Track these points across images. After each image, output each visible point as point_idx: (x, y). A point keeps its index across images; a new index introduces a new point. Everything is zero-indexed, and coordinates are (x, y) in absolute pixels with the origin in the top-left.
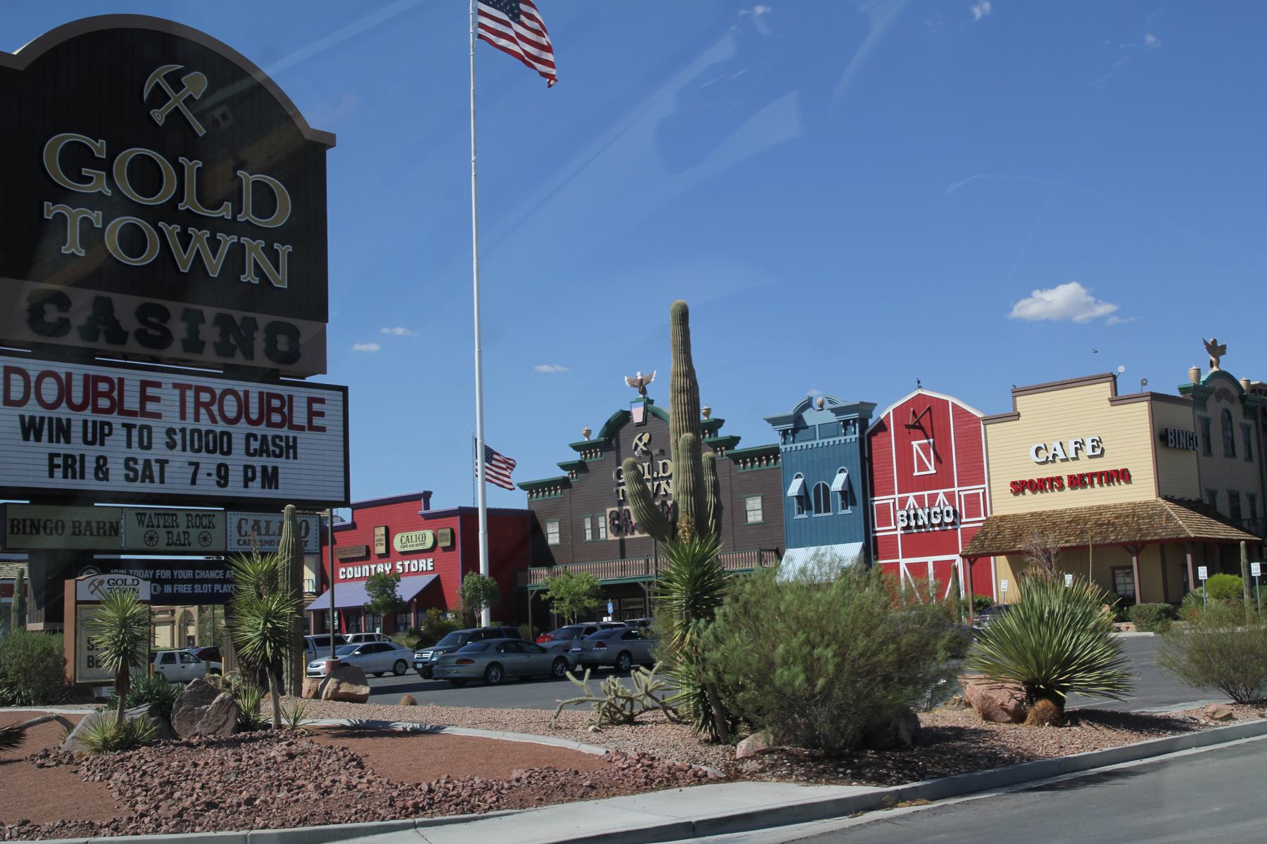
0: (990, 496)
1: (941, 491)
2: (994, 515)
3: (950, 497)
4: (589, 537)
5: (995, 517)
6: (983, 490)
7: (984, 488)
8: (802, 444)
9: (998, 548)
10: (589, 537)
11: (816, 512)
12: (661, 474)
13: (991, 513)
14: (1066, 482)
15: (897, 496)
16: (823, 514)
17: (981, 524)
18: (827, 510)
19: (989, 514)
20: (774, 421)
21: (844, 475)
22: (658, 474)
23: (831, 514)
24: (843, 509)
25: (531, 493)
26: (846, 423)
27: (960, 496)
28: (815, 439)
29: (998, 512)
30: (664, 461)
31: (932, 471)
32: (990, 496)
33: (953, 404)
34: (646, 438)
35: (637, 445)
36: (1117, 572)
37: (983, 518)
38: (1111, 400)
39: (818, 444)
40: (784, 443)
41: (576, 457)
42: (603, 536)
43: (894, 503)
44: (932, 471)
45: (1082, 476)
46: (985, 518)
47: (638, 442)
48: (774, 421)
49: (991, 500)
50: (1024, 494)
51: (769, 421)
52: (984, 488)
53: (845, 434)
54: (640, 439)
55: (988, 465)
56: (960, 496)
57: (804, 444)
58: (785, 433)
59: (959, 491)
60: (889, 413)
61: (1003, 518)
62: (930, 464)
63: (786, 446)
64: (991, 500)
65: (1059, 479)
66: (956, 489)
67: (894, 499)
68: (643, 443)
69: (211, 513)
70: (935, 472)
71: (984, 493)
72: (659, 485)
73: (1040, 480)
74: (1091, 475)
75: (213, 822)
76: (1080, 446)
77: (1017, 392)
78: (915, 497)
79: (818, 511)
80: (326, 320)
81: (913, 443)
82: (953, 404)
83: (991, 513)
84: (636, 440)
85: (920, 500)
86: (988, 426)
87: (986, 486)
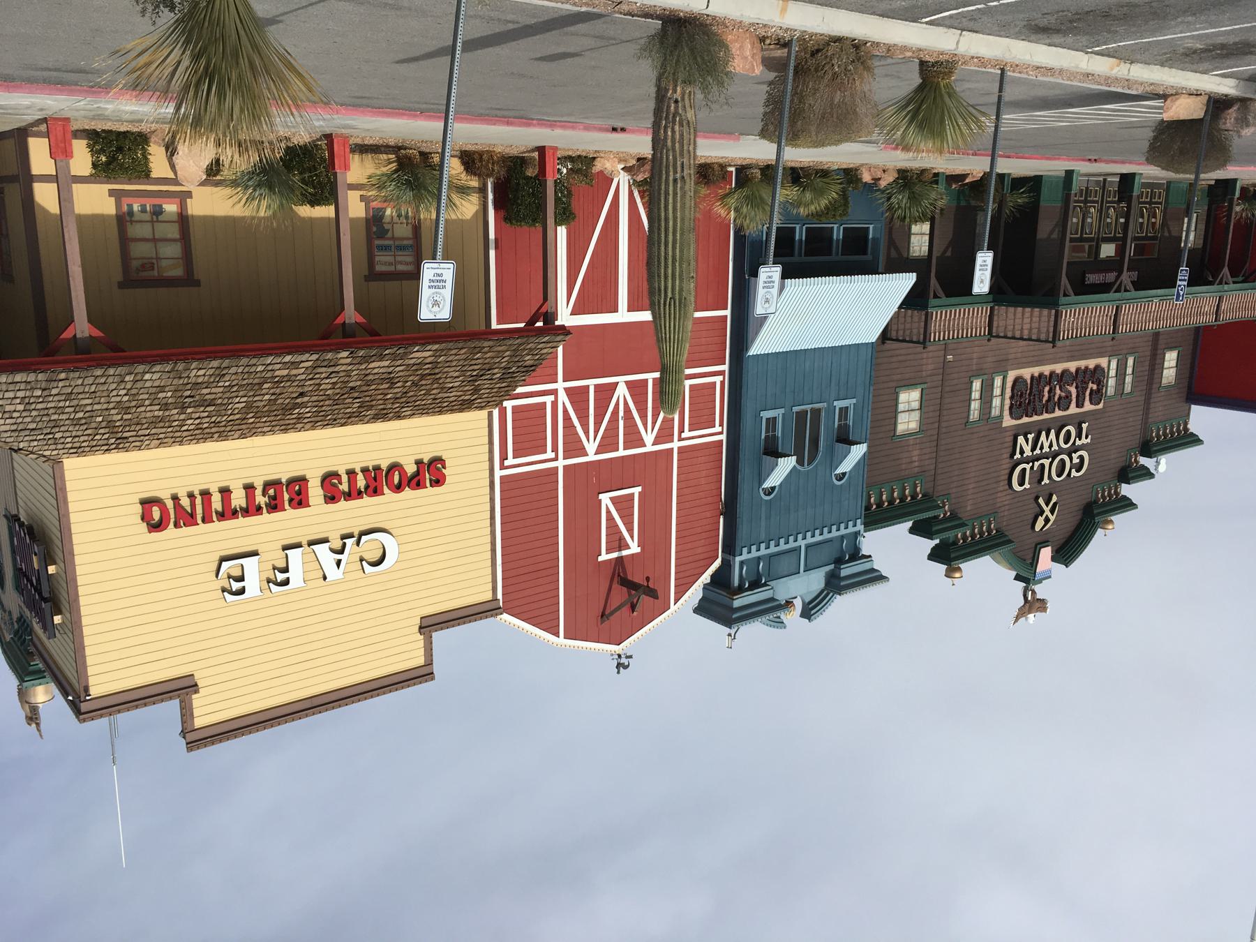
0: (491, 451)
1: (592, 457)
2: (484, 413)
3: (574, 447)
4: (1130, 362)
5: (481, 408)
6: (507, 463)
7: (502, 467)
8: (830, 536)
9: (474, 350)
10: (1130, 362)
11: (819, 410)
12: (1028, 467)
13: (490, 415)
14: (315, 492)
15: (675, 445)
16: (808, 407)
17: (520, 390)
18: (801, 416)
19: (496, 412)
20: (874, 577)
21: (767, 484)
22: (1032, 468)
23: (795, 409)
24: (775, 418)
25: (1186, 429)
26: (756, 584)
27: (555, 449)
28: (807, 547)
29: (475, 420)
30: (1022, 488)
31: (605, 498)
32: (491, 451)
33: (557, 634)
34: (1040, 522)
35: (1052, 512)
36: (178, 272)
37: (509, 404)
38: (194, 687)
39: (804, 538)
40: (857, 534)
41: (1126, 490)
42: (1114, 364)
43: (681, 431)
44: (605, 498)
45: (274, 506)
46: (505, 404)
47: (1050, 515)
48: (874, 577)
49: (491, 443)
50: (419, 463)
51: (880, 578)
52: (502, 467)
53: (759, 558)
54: (1047, 520)
55: (492, 518)
56: (555, 449)
57: (826, 536)
58: (856, 555)
59: (556, 459)
60: (676, 602)
61: (465, 406)
62: (608, 512)
63: (856, 529)
64: (491, 443)
65: (331, 497)
66: (561, 463)
67: (680, 439)
68: (1044, 516)
69: (787, 222)
70: (601, 496)
71: (504, 457)
72: (1033, 449)
73: (376, 492)
74: (251, 510)
75: (852, 119)
76: (279, 578)
77: (423, 674)
78: (629, 385)
79: (816, 413)
80: (545, 147)
81: (638, 550)
82: (557, 634)
83: (490, 415)
84: (1052, 518)
85: (634, 439)
86: (489, 596)
87: (498, 473)
